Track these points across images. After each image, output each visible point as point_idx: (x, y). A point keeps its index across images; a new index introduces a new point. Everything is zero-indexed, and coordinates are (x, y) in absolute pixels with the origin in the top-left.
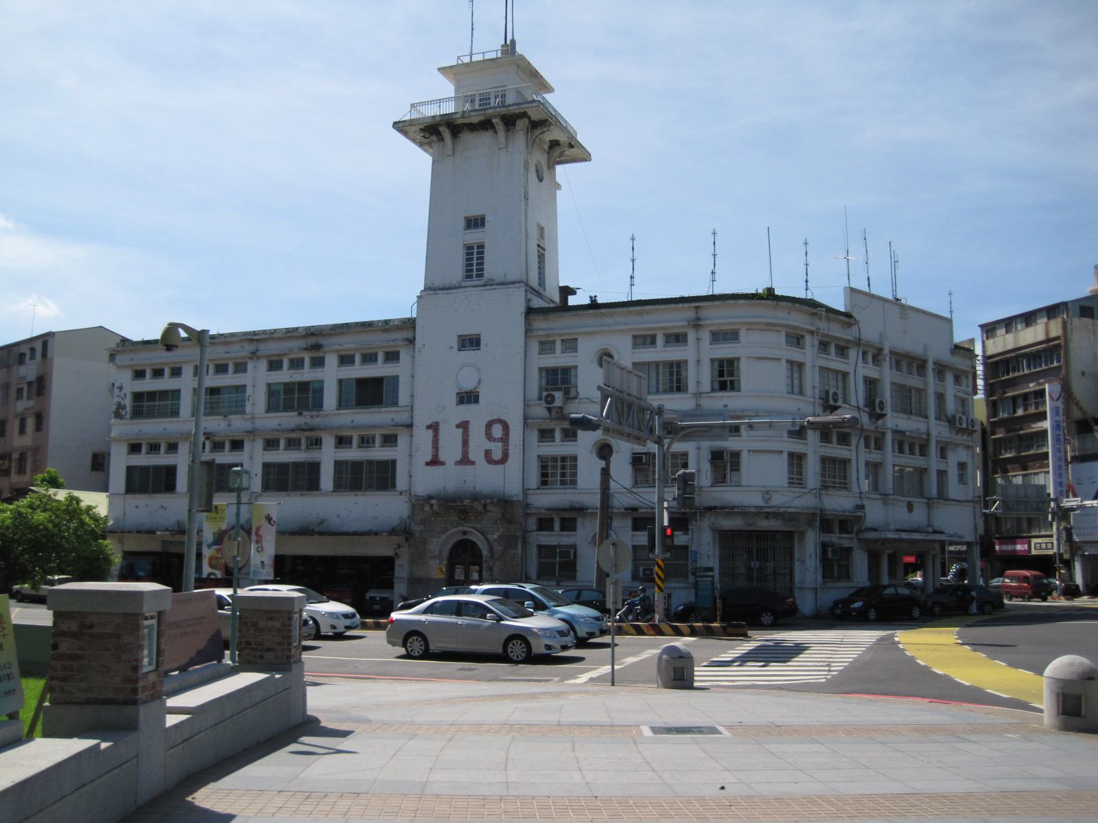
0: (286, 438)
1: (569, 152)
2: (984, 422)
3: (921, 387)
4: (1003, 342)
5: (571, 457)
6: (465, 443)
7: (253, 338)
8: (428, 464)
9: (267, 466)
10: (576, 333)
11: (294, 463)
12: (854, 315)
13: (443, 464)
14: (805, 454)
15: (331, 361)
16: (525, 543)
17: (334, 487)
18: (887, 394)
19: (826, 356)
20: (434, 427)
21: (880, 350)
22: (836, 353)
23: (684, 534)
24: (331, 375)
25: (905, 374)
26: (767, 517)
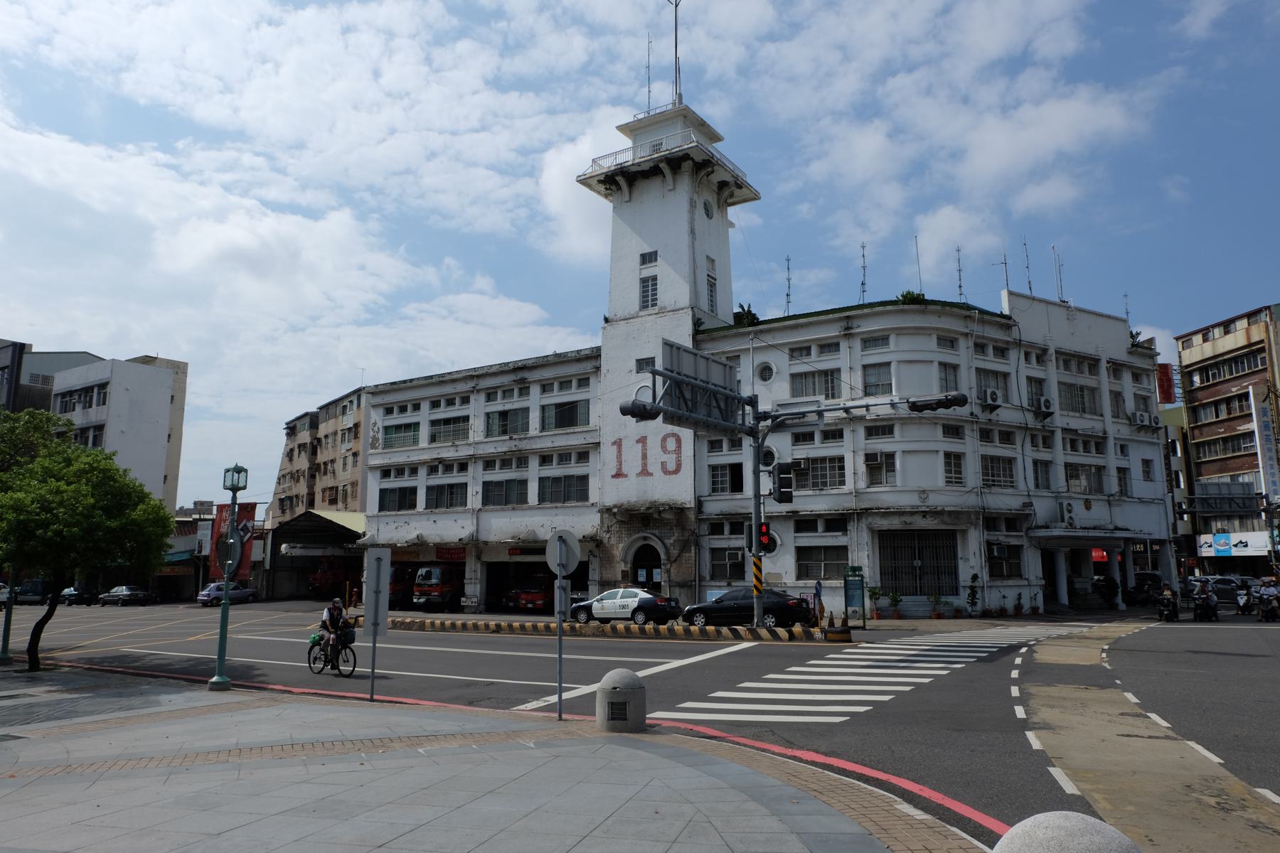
1: (737, 192)
2: (1186, 426)
3: (1095, 386)
4: (1199, 351)
5: (721, 467)
6: (644, 457)
7: (474, 376)
8: (613, 477)
11: (507, 481)
12: (1013, 317)
13: (626, 476)
14: (964, 454)
15: (535, 390)
16: (697, 545)
17: (539, 501)
18: (1053, 392)
19: (982, 357)
20: (618, 443)
21: (1045, 351)
22: (994, 355)
23: (843, 535)
24: (535, 401)
26: (924, 517)
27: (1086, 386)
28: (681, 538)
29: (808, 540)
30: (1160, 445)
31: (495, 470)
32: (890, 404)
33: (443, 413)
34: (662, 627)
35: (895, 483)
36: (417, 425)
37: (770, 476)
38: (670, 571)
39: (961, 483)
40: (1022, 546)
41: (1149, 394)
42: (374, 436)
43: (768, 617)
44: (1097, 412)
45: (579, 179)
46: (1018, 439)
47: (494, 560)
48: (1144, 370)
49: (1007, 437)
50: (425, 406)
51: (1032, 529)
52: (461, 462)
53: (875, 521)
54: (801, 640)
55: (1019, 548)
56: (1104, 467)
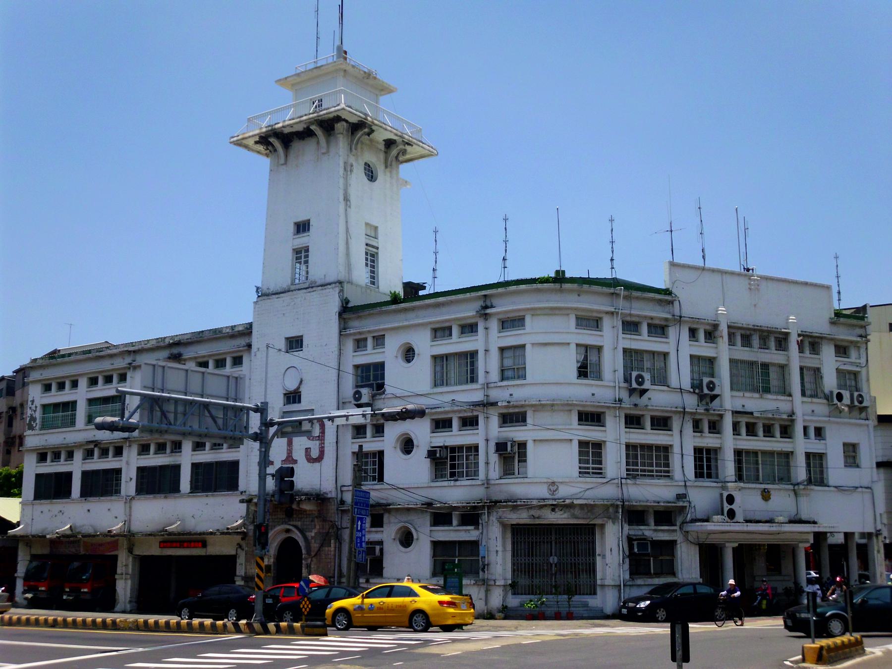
0: (156, 443)
9: (141, 470)
10: (383, 330)
12: (674, 291)
17: (191, 488)
23: (475, 529)
25: (756, 350)
26: (553, 510)
27: (770, 363)
28: (321, 531)
29: (445, 534)
30: (870, 426)
31: (149, 454)
32: (362, 414)
33: (103, 391)
34: (220, 623)
35: (526, 474)
36: (74, 403)
37: (273, 479)
38: (310, 567)
39: (601, 473)
40: (676, 541)
41: (858, 369)
42: (31, 415)
43: (289, 613)
44: (785, 391)
45: (232, 140)
46: (676, 424)
47: (145, 554)
48: (852, 342)
49: (661, 423)
50: (83, 383)
51: (687, 523)
52: (117, 445)
53: (505, 515)
54: (285, 634)
55: (672, 544)
56: (792, 452)
